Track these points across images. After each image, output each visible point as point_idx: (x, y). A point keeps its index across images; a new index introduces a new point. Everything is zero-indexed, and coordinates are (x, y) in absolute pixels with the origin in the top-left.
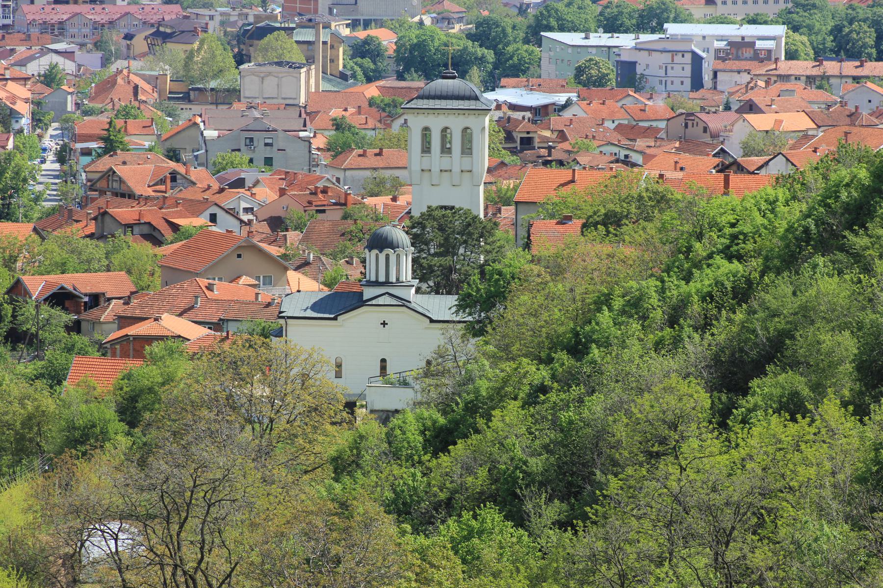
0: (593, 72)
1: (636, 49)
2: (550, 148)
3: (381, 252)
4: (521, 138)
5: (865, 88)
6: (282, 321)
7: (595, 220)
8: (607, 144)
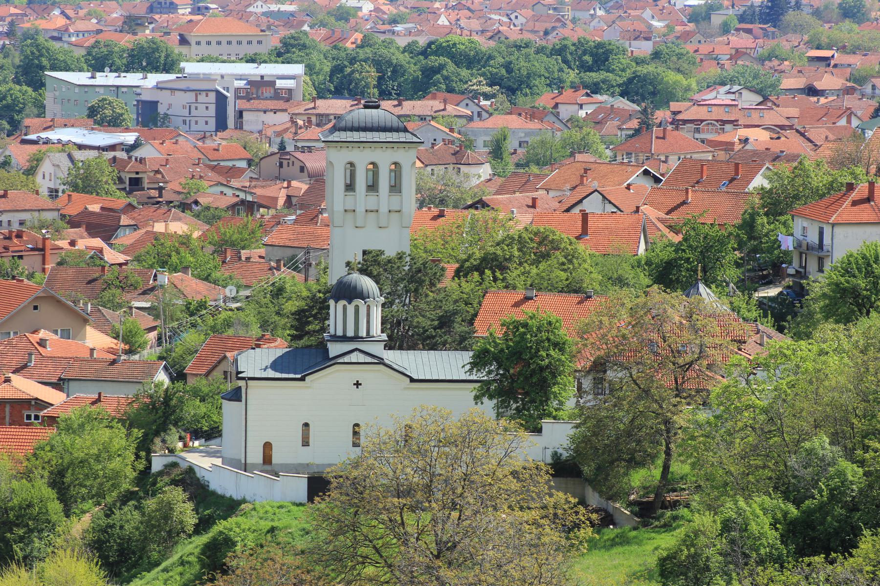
0: (107, 112)
1: (158, 88)
2: (160, 189)
3: (350, 303)
4: (130, 179)
5: (430, 127)
6: (241, 383)
7: (471, 263)
8: (216, 185)
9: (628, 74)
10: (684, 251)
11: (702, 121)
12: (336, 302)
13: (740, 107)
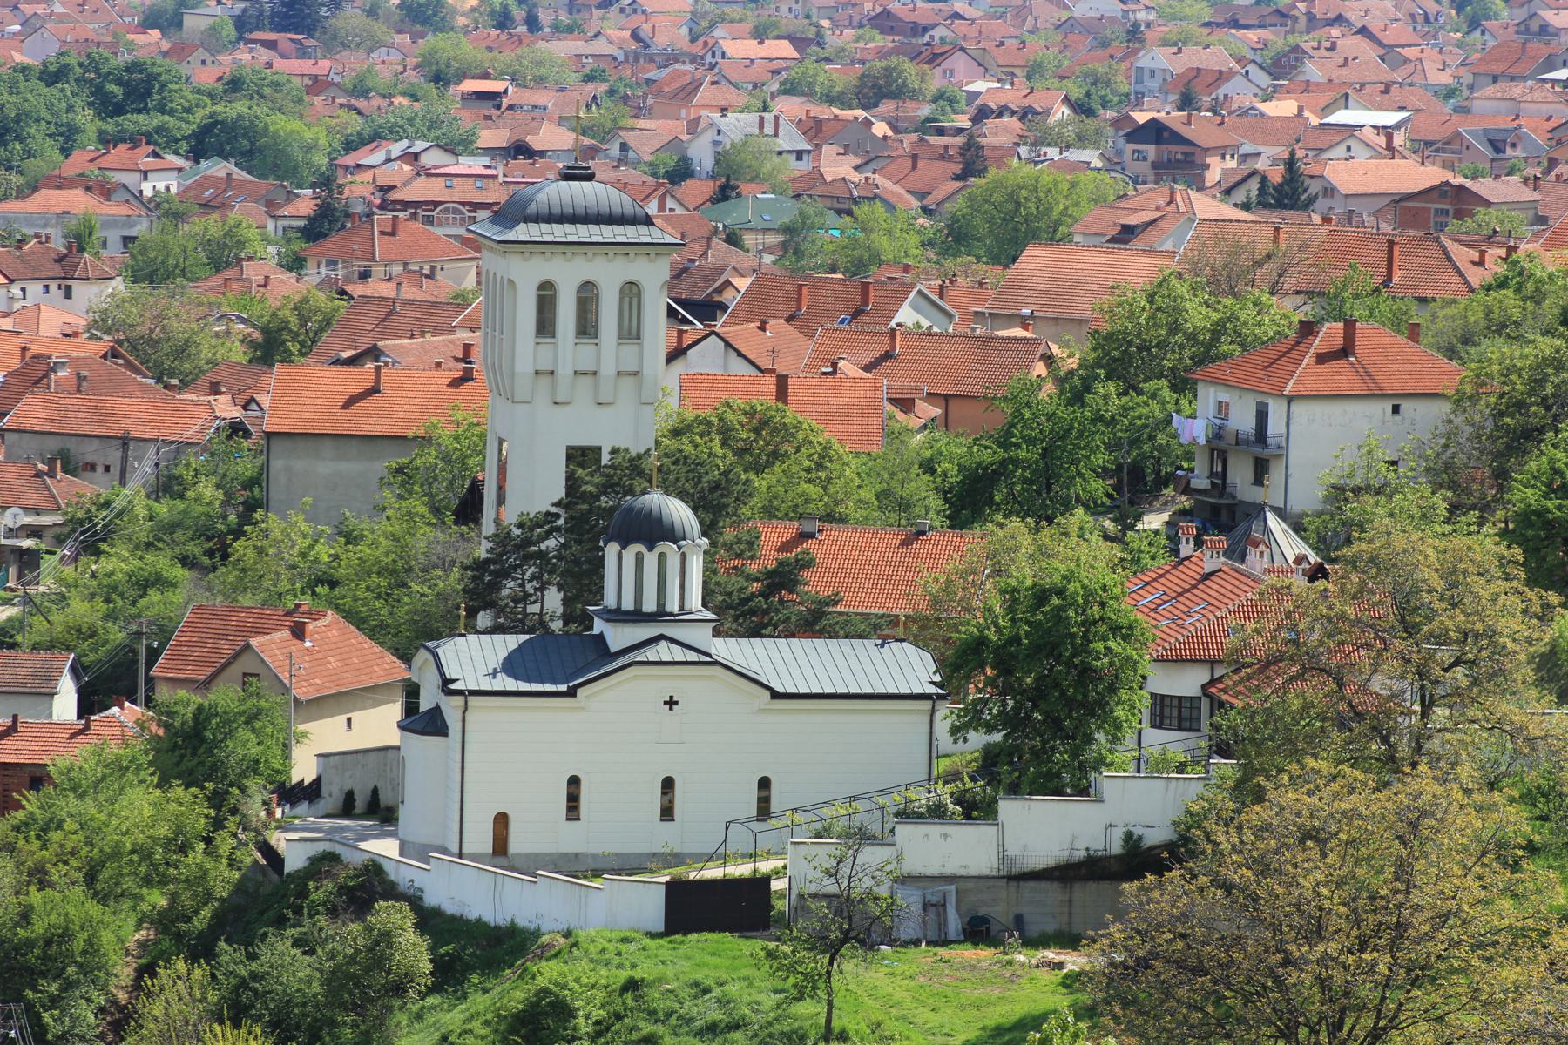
3: (651, 549)
9: (200, 116)
10: (1018, 446)
11: (436, 204)
12: (624, 548)
13: (501, 179)
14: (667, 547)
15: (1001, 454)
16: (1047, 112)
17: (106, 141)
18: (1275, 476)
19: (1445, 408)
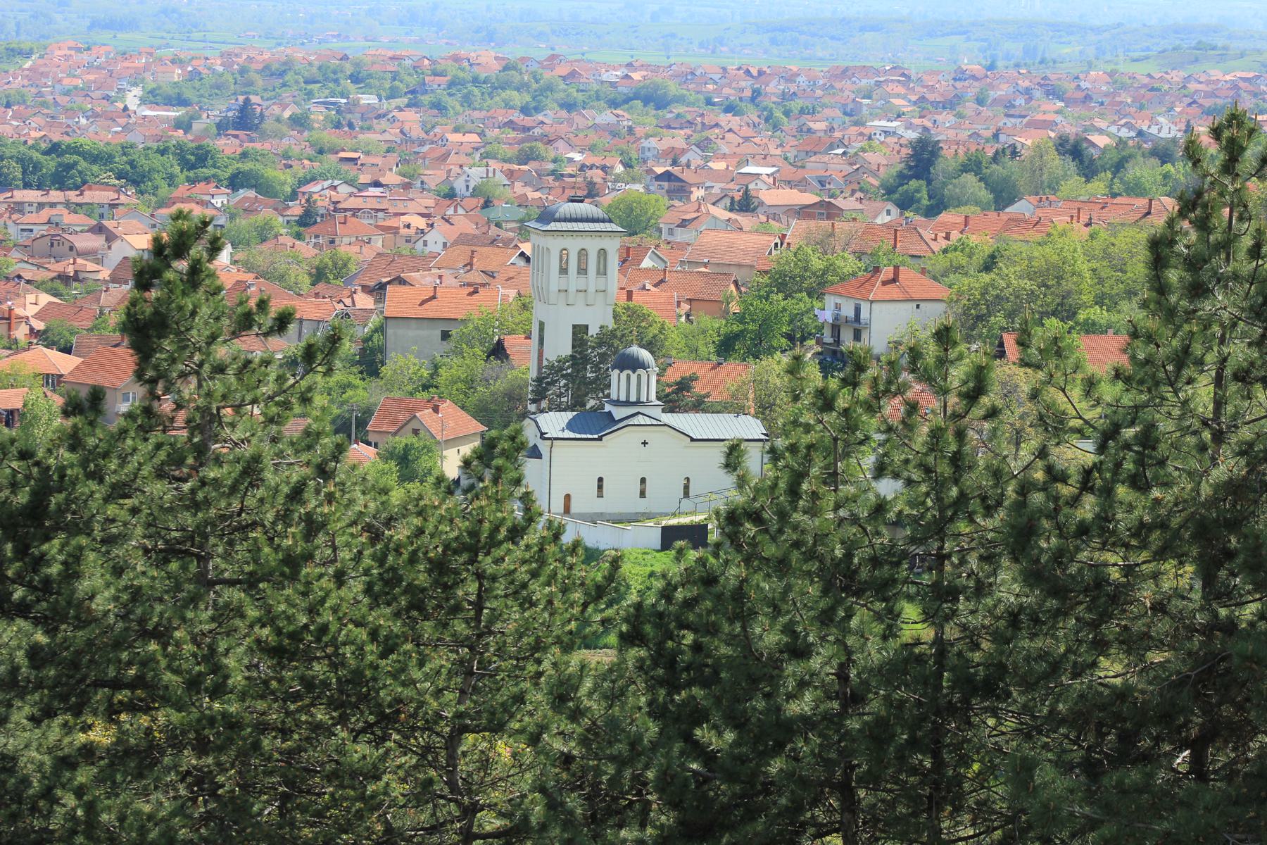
9: (230, 170)
14: (640, 371)
15: (741, 327)
16: (612, 167)
17: (193, 181)
18: (864, 336)
19: (941, 307)
